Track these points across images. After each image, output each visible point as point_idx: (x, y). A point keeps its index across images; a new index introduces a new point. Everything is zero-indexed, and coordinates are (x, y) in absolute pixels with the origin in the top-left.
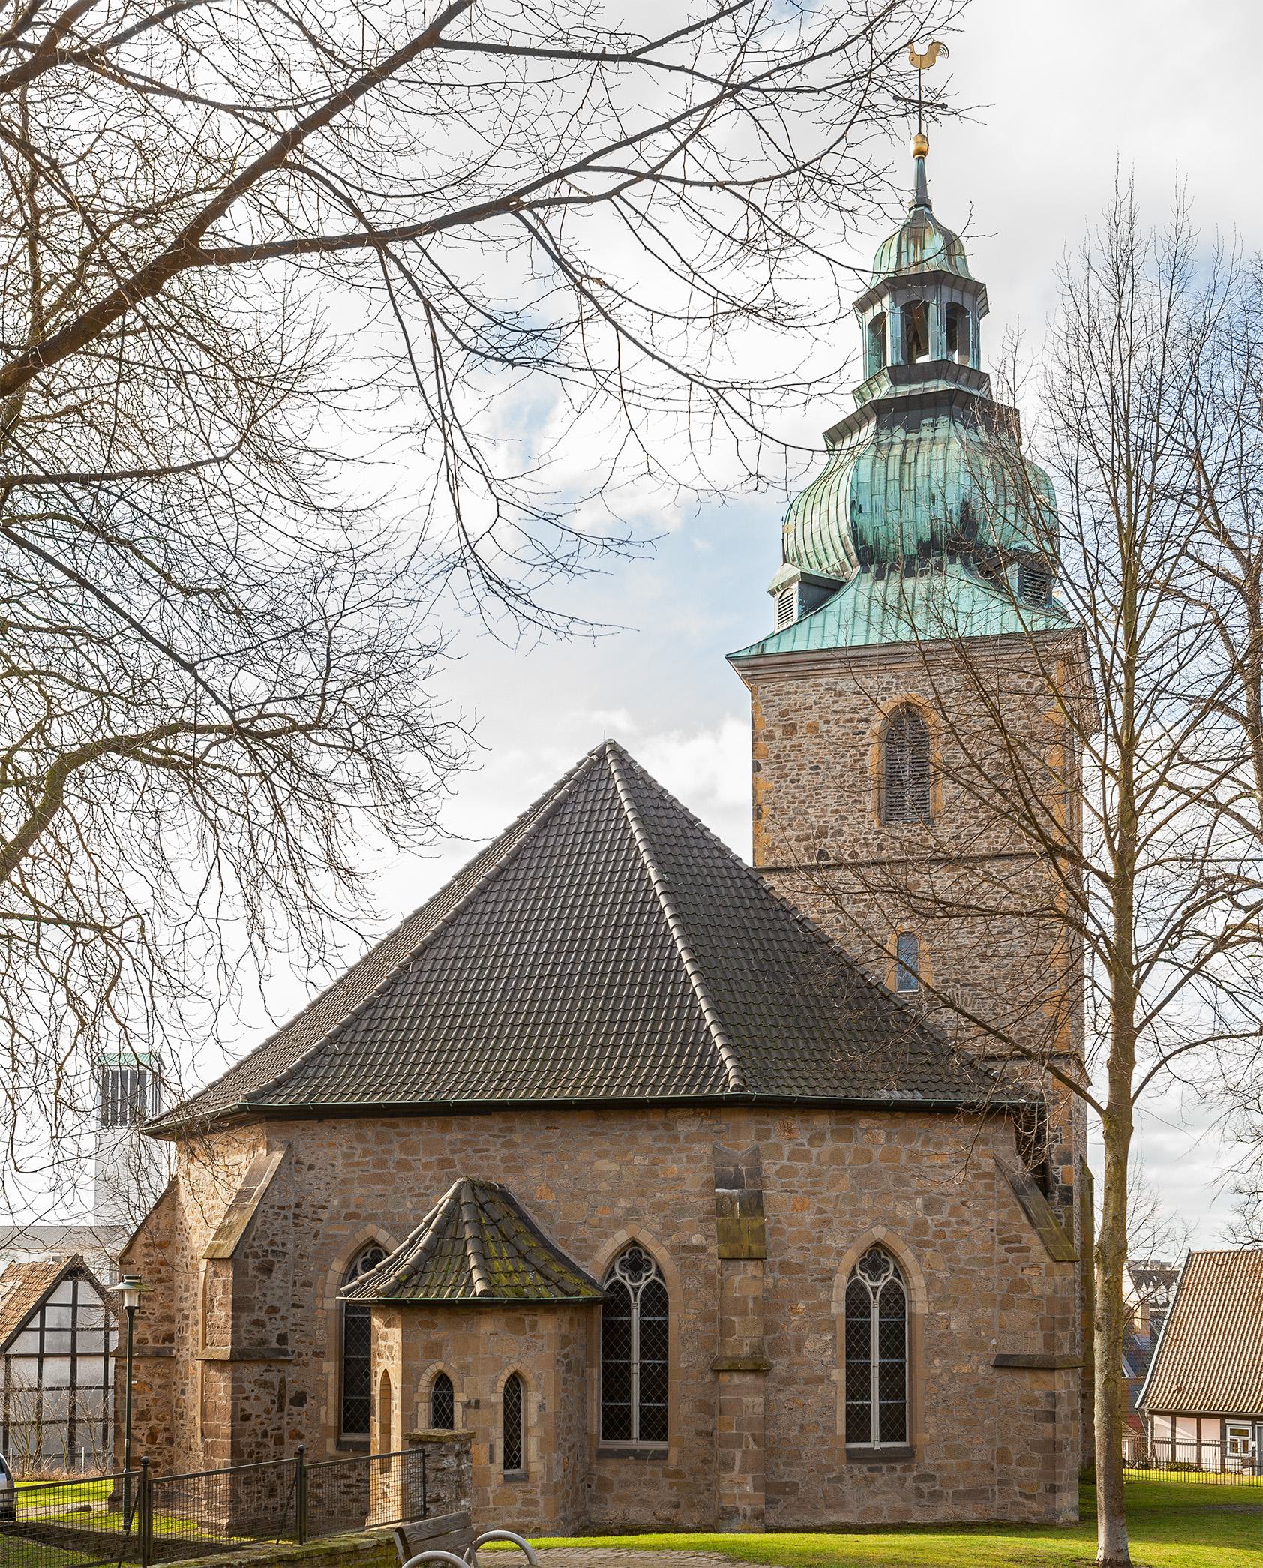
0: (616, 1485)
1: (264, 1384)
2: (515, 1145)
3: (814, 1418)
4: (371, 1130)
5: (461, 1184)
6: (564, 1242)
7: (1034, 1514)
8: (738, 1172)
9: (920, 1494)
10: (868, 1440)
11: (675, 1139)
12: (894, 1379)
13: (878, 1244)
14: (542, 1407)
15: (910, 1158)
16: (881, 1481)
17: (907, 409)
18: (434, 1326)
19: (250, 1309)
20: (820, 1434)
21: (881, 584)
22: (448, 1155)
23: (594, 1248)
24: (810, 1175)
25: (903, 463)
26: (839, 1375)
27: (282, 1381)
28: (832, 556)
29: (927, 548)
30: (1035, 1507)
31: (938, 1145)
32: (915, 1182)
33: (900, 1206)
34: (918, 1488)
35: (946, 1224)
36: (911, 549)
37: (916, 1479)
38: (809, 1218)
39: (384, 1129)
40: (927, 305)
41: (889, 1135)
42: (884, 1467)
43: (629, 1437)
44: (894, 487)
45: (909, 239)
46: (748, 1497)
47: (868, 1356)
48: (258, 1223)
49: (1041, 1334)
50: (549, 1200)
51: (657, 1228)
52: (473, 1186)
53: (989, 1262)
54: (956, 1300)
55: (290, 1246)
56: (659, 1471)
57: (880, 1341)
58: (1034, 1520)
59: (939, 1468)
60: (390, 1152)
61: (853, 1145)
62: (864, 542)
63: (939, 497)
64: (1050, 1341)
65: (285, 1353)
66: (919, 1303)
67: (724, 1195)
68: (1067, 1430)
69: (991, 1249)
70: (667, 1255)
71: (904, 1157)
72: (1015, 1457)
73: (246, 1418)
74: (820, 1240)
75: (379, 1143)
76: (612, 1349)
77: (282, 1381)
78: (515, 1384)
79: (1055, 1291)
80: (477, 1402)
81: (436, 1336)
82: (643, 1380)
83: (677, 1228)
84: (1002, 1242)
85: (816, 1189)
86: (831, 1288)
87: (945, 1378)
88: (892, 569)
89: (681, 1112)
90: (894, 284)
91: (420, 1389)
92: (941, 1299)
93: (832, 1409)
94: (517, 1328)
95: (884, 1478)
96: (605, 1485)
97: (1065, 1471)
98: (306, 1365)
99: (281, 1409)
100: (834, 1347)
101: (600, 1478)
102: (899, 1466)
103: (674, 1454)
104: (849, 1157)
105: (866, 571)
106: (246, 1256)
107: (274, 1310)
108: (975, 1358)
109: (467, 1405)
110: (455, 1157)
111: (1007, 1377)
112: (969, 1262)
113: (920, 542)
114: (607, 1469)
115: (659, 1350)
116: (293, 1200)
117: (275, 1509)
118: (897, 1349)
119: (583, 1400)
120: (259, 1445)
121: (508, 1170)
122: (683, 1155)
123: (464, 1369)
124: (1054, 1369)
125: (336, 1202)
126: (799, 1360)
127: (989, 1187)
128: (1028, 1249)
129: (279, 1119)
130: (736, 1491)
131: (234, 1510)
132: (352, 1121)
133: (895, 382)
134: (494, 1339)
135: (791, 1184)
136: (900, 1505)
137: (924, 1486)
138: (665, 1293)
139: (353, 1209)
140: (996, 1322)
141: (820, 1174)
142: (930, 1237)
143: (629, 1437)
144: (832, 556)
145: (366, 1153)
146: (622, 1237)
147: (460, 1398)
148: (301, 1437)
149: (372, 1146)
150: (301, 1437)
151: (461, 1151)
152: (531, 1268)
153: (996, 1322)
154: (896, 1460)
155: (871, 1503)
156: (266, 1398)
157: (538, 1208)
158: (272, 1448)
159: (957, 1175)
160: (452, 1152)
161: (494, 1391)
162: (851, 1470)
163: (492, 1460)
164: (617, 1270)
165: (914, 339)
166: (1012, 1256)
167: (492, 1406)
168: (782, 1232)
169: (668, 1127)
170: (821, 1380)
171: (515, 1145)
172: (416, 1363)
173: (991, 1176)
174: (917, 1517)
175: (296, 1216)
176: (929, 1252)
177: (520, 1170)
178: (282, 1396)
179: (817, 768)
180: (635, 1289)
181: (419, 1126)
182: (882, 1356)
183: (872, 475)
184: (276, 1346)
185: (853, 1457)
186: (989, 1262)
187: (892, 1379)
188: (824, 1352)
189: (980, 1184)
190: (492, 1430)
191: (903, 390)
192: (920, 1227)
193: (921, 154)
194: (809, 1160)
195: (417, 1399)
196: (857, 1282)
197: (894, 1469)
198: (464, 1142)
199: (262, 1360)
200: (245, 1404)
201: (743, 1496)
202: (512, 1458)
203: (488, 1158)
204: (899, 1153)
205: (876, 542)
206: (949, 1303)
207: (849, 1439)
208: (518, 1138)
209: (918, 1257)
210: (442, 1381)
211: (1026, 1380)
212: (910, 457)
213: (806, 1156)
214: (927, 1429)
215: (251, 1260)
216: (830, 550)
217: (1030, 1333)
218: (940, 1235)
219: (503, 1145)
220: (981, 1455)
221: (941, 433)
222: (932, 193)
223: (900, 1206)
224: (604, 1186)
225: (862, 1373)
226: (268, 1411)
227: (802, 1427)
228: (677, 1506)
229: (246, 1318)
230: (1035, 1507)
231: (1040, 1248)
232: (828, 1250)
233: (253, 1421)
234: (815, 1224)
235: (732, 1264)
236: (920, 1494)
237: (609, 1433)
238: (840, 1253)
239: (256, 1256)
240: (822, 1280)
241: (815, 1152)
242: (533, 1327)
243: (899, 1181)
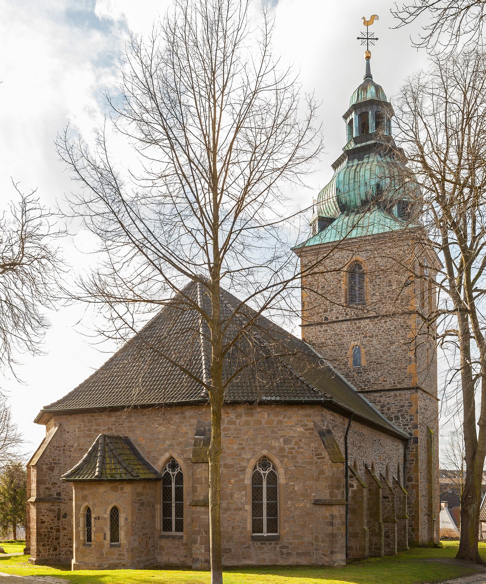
0: (166, 549)
1: (51, 510)
2: (132, 422)
3: (238, 524)
4: (87, 418)
5: (100, 436)
6: (148, 457)
7: (326, 562)
8: (205, 429)
9: (282, 554)
10: (262, 532)
11: (185, 418)
12: (273, 510)
13: (264, 457)
14: (126, 519)
15: (277, 423)
16: (266, 548)
17: (359, 152)
18: (85, 489)
19: (44, 483)
20: (240, 530)
21: (347, 218)
22: (111, 426)
23: (158, 460)
24: (236, 430)
25: (355, 172)
26: (248, 508)
27: (59, 509)
28: (331, 209)
29: (364, 203)
30: (327, 559)
31: (289, 418)
32: (280, 432)
33: (273, 442)
34: (281, 551)
35: (293, 448)
36: (359, 204)
37: (280, 547)
38: (236, 447)
39: (90, 418)
40: (368, 113)
41: (269, 414)
42: (267, 543)
43: (171, 531)
44: (352, 181)
45: (362, 89)
46: (202, 554)
47: (262, 500)
48: (47, 453)
49: (329, 491)
50: (143, 442)
51: (179, 452)
52: (104, 437)
53: (311, 463)
54: (297, 478)
55: (62, 461)
56: (180, 543)
57: (266, 494)
58: (326, 564)
59: (290, 543)
60: (92, 426)
61: (254, 418)
62: (341, 203)
63: (368, 183)
64: (331, 494)
65: (60, 499)
66: (282, 480)
67: (198, 438)
68: (339, 529)
69: (312, 458)
70: (182, 462)
71: (275, 423)
72: (320, 540)
73: (43, 522)
74: (240, 455)
75: (89, 422)
76: (166, 498)
77: (59, 509)
78: (115, 512)
79: (333, 474)
80: (99, 517)
81: (85, 492)
82: (176, 509)
83: (186, 451)
84: (316, 455)
85: (239, 436)
86: (244, 474)
87: (293, 509)
88: (353, 211)
89: (187, 407)
90: (355, 107)
91: (81, 513)
92: (291, 477)
93: (246, 520)
94: (115, 489)
95: (267, 547)
96: (162, 548)
97: (338, 545)
98: (67, 503)
99: (59, 519)
100: (246, 496)
101: (161, 546)
102: (273, 543)
103: (185, 537)
104: (252, 423)
105: (343, 213)
106: (42, 464)
107: (55, 484)
108: (305, 501)
109: (95, 518)
110: (113, 427)
111: (318, 508)
112: (303, 463)
113: (362, 201)
114: (163, 543)
115: (169, 498)
116: (63, 444)
117: (56, 555)
118: (274, 497)
119: (154, 517)
120: (49, 532)
121: (130, 431)
122: (188, 424)
123: (94, 505)
124: (332, 505)
125: (76, 445)
126: (231, 501)
127: (311, 434)
128: (324, 458)
129: (58, 415)
130: (198, 552)
131: (38, 555)
132: (80, 415)
133: (356, 143)
134: (106, 494)
135: (228, 434)
136: (273, 557)
137: (284, 550)
138: (276, 476)
139: (81, 447)
140: (314, 486)
141: (240, 430)
142: (286, 454)
143: (171, 531)
144: (331, 209)
145: (85, 426)
146: (167, 455)
147: (93, 516)
148: (65, 529)
149: (87, 424)
150: (65, 529)
151: (115, 425)
152: (122, 467)
153: (314, 486)
154: (272, 540)
155: (262, 557)
156: (52, 515)
157: (139, 445)
158: (55, 533)
159: (300, 429)
160: (112, 425)
161: (105, 513)
162: (253, 544)
163: (105, 539)
164: (167, 468)
165: (364, 126)
166: (319, 461)
167: (105, 519)
168: (225, 453)
169: (183, 413)
170: (241, 509)
171: (132, 422)
172: (79, 503)
173: (312, 429)
174: (281, 562)
175: (64, 450)
176: (286, 459)
177: (133, 431)
178: (59, 514)
179: (324, 287)
180: (173, 475)
181: (101, 416)
182: (268, 500)
183: (344, 177)
184: (56, 497)
185: (254, 539)
186: (311, 463)
187: (272, 509)
188: (243, 499)
189: (307, 433)
190: (105, 528)
191: (359, 145)
192: (282, 450)
193: (368, 58)
194: (236, 425)
195: (80, 516)
196: (257, 471)
197: (271, 544)
198: (116, 421)
199: (49, 501)
200: (42, 518)
201: (201, 554)
202: (115, 537)
203: (123, 427)
204: (273, 421)
205: (346, 203)
206: (294, 479)
207: (254, 532)
208: (133, 419)
209: (281, 462)
210: (89, 510)
211: (324, 509)
212: (358, 170)
213: (234, 423)
214: (285, 528)
215: (44, 466)
216: (331, 208)
217: (325, 491)
218: (291, 453)
219: (128, 422)
220: (308, 538)
221: (371, 160)
222: (372, 73)
223: (273, 442)
224: (161, 436)
225: (259, 506)
226: (53, 520)
227: (233, 527)
228: (186, 557)
229: (42, 486)
230: (327, 559)
231: (328, 457)
232: (243, 460)
233: (46, 523)
234: (238, 449)
235: (196, 465)
236: (282, 554)
237: (165, 529)
238: (248, 460)
239: (47, 464)
240: (241, 471)
241: (238, 421)
242: (122, 489)
243: (273, 432)
